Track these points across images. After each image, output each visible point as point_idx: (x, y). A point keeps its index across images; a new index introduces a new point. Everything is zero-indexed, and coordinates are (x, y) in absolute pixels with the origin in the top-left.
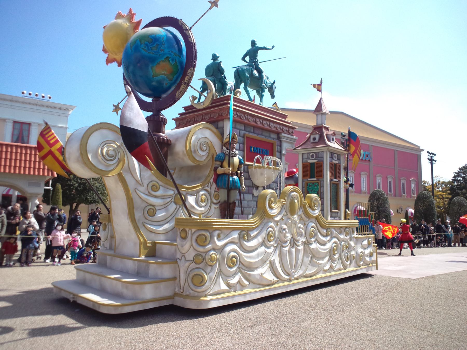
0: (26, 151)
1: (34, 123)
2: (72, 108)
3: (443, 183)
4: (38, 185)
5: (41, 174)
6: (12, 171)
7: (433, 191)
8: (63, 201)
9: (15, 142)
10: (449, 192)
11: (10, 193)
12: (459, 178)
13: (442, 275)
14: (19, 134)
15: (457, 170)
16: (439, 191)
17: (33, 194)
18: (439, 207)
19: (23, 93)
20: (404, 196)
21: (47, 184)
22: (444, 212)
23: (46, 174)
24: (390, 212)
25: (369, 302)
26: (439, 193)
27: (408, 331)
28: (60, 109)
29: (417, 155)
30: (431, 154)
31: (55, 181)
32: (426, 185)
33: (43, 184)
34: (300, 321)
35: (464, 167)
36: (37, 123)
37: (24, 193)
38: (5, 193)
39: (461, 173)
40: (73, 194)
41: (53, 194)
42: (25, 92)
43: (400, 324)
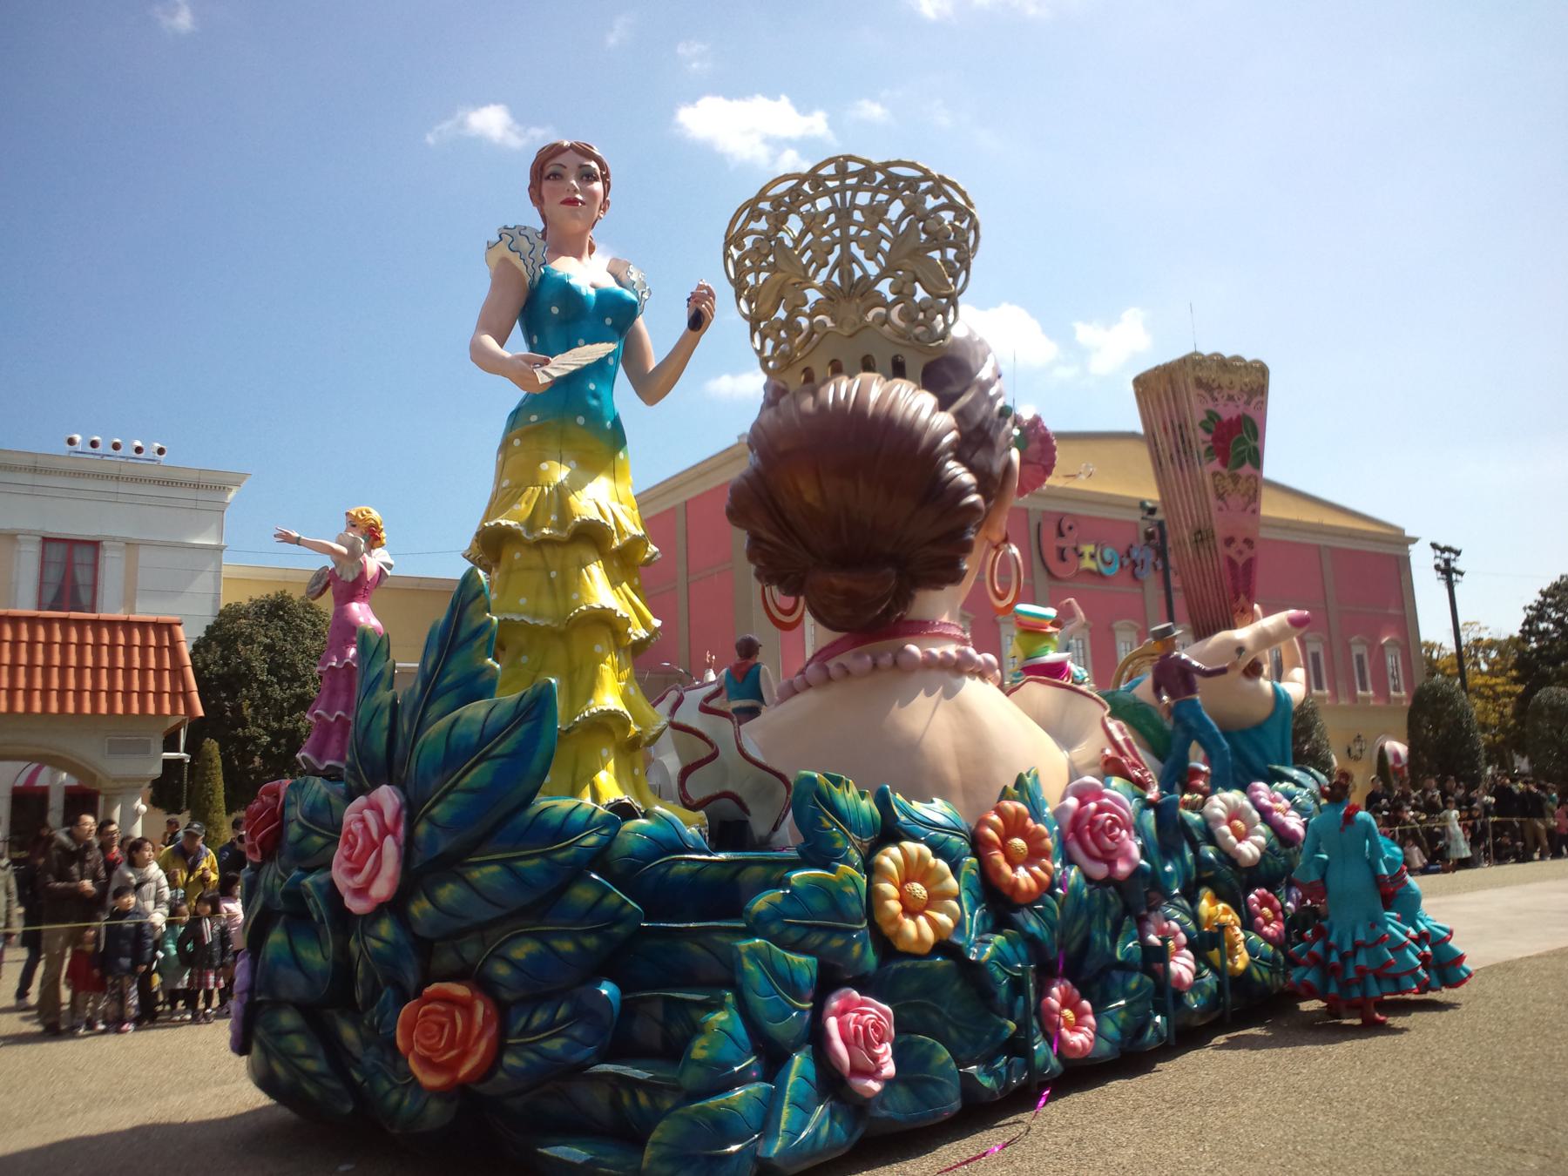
0: (97, 636)
1: (114, 539)
2: (237, 479)
3: (1492, 644)
4: (143, 749)
5: (152, 709)
6: (54, 707)
7: (1462, 673)
8: (226, 797)
9: (51, 608)
10: (1514, 673)
11: (42, 780)
12: (1542, 626)
13: (1539, 957)
14: (63, 579)
15: (1533, 598)
16: (1481, 673)
17: (126, 780)
18: (1484, 727)
19: (71, 442)
20: (1366, 699)
21: (171, 743)
22: (1504, 742)
23: (167, 709)
24: (1328, 757)
25: (1314, 1065)
26: (1479, 681)
27: (1471, 1157)
28: (197, 486)
29: (1397, 558)
30: (1443, 550)
31: (198, 730)
32: (1435, 655)
33: (157, 742)
34: (1103, 1150)
35: (1556, 587)
36: (122, 539)
37: (93, 777)
38: (21, 782)
39: (1550, 605)
40: (254, 771)
41: (191, 776)
42: (78, 438)
43: (1439, 1136)
